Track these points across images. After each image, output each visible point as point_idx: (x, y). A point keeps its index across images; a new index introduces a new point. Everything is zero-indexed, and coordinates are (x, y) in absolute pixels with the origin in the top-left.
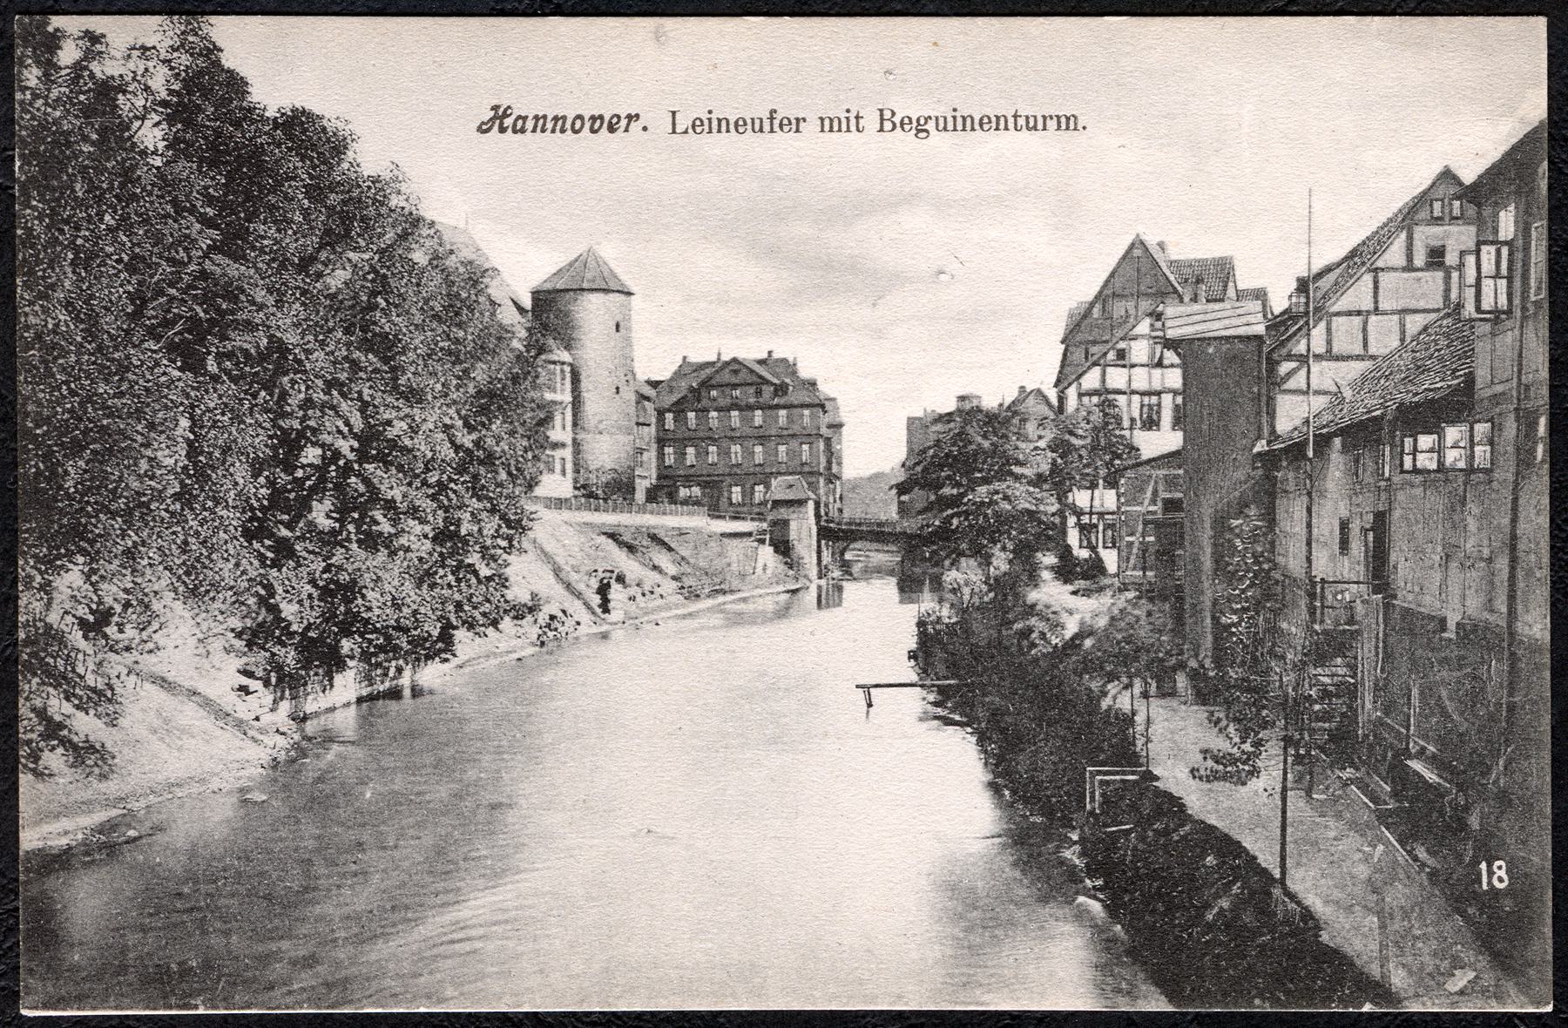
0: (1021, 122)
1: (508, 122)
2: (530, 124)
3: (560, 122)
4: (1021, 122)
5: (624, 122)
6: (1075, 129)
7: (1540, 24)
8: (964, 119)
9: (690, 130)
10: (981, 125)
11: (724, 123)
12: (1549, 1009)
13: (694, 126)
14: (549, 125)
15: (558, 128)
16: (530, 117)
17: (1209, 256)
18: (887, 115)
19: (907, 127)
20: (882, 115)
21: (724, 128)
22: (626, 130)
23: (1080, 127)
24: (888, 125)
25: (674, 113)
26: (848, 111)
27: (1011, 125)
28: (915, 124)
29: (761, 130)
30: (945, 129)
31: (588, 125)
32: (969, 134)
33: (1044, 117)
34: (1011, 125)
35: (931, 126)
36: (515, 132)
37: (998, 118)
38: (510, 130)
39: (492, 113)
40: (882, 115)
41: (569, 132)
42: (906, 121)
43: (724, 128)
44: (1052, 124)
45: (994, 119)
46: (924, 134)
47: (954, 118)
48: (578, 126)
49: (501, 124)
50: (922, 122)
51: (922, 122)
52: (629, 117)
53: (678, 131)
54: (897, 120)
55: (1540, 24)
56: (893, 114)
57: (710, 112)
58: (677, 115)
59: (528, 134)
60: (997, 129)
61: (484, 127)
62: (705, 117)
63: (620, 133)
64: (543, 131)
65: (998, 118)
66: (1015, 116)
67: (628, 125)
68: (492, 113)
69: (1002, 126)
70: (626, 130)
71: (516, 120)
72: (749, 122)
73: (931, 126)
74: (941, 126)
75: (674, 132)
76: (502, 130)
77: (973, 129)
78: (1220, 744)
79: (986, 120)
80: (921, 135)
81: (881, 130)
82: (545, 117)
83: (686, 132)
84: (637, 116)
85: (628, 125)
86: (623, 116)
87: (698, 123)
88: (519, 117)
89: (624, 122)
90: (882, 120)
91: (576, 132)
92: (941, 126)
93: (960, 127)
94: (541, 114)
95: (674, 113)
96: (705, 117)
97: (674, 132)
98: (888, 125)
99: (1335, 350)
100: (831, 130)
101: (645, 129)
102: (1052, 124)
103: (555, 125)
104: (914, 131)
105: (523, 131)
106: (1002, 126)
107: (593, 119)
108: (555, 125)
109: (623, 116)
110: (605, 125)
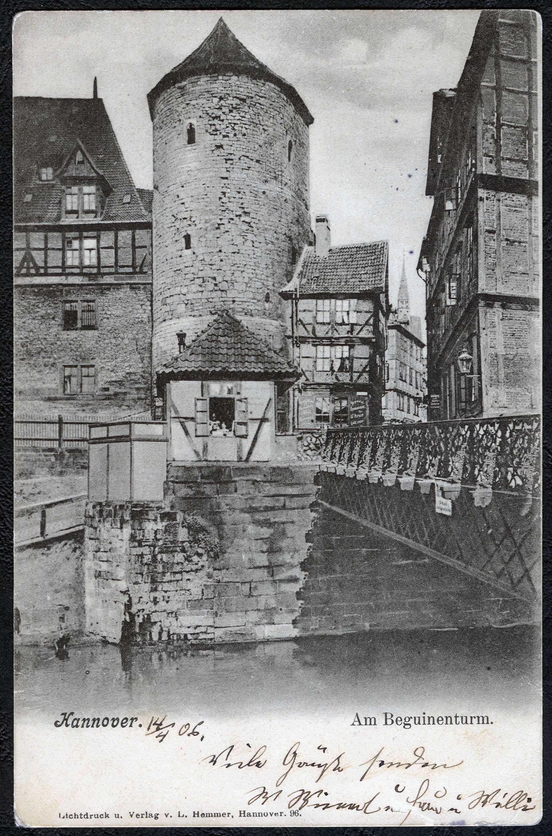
0: (459, 719)
2: (80, 723)
4: (459, 719)
6: (488, 723)
7: (18, 824)
8: (429, 718)
10: (438, 721)
11: (431, 719)
14: (91, 723)
16: (81, 719)
17: (299, 93)
18: (389, 716)
19: (399, 723)
20: (386, 716)
21: (431, 722)
22: (131, 726)
23: (490, 722)
24: (389, 722)
27: (454, 721)
28: (403, 721)
29: (419, 723)
30: (419, 723)
31: (110, 722)
33: (471, 718)
34: (454, 721)
35: (412, 722)
37: (447, 718)
38: (70, 726)
40: (386, 716)
41: (101, 726)
42: (399, 719)
43: (431, 722)
44: (475, 721)
45: (445, 719)
46: (408, 726)
47: (424, 717)
50: (407, 719)
51: (407, 719)
54: (394, 719)
55: (18, 824)
56: (392, 716)
60: (447, 723)
61: (58, 723)
64: (88, 727)
66: (456, 717)
69: (449, 722)
72: (403, 719)
73: (412, 722)
74: (417, 722)
80: (406, 727)
81: (386, 724)
84: (136, 719)
86: (129, 718)
87: (440, 719)
89: (129, 722)
90: (386, 719)
92: (417, 722)
93: (427, 722)
98: (389, 722)
99: (61, 247)
101: (492, 723)
102: (475, 721)
103: (94, 723)
104: (403, 725)
105: (77, 726)
106: (449, 722)
107: (113, 720)
108: (94, 723)
109: (129, 718)
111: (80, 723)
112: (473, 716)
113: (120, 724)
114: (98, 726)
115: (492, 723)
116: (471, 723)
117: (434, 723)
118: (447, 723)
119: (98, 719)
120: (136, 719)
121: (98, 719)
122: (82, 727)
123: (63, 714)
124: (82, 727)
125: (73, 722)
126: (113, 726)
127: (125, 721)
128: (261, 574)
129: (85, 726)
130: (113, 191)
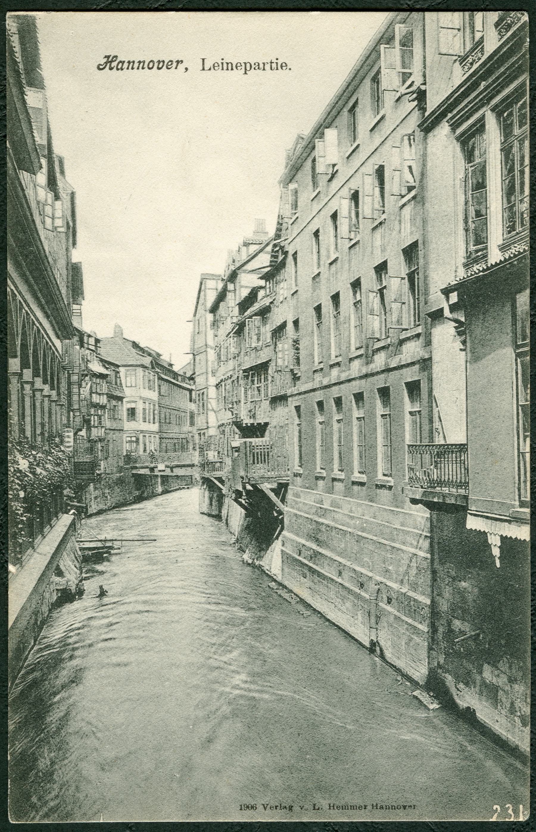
1: (114, 64)
2: (126, 65)
3: (142, 64)
5: (175, 64)
8: (227, 64)
9: (212, 68)
10: (282, 67)
12: (523, 817)
13: (214, 67)
14: (136, 65)
15: (141, 67)
22: (176, 68)
25: (203, 60)
26: (277, 59)
32: (230, 71)
33: (264, 64)
36: (118, 69)
37: (245, 63)
38: (115, 68)
39: (106, 60)
41: (146, 68)
45: (243, 65)
47: (222, 63)
48: (151, 66)
49: (110, 65)
52: (178, 62)
53: (206, 69)
57: (223, 59)
58: (205, 60)
59: (125, 70)
61: (101, 67)
62: (220, 62)
63: (173, 69)
64: (143, 68)
65: (245, 63)
67: (177, 65)
68: (106, 60)
70: (176, 68)
71: (119, 63)
75: (203, 69)
76: (111, 69)
77: (232, 69)
78: (246, 589)
79: (239, 65)
82: (134, 62)
83: (210, 69)
84: (182, 61)
85: (177, 65)
86: (174, 61)
87: (216, 65)
88: (121, 62)
89: (175, 64)
91: (149, 68)
94: (131, 61)
95: (203, 60)
96: (220, 62)
97: (203, 69)
100: (227, 69)
101: (290, 69)
109: (174, 61)
110: (166, 64)
111: (126, 65)
112: (265, 61)
113: (165, 67)
114: (133, 68)
115: (290, 69)
116: (264, 69)
117: (232, 69)
118: (223, 69)
119: (144, 62)
120: (182, 61)
121: (144, 62)
122: (138, 68)
123: (106, 57)
124: (138, 68)
125: (153, 65)
126: (159, 68)
127: (170, 63)
128: (13, 595)
129: (141, 67)
130: (503, 306)
